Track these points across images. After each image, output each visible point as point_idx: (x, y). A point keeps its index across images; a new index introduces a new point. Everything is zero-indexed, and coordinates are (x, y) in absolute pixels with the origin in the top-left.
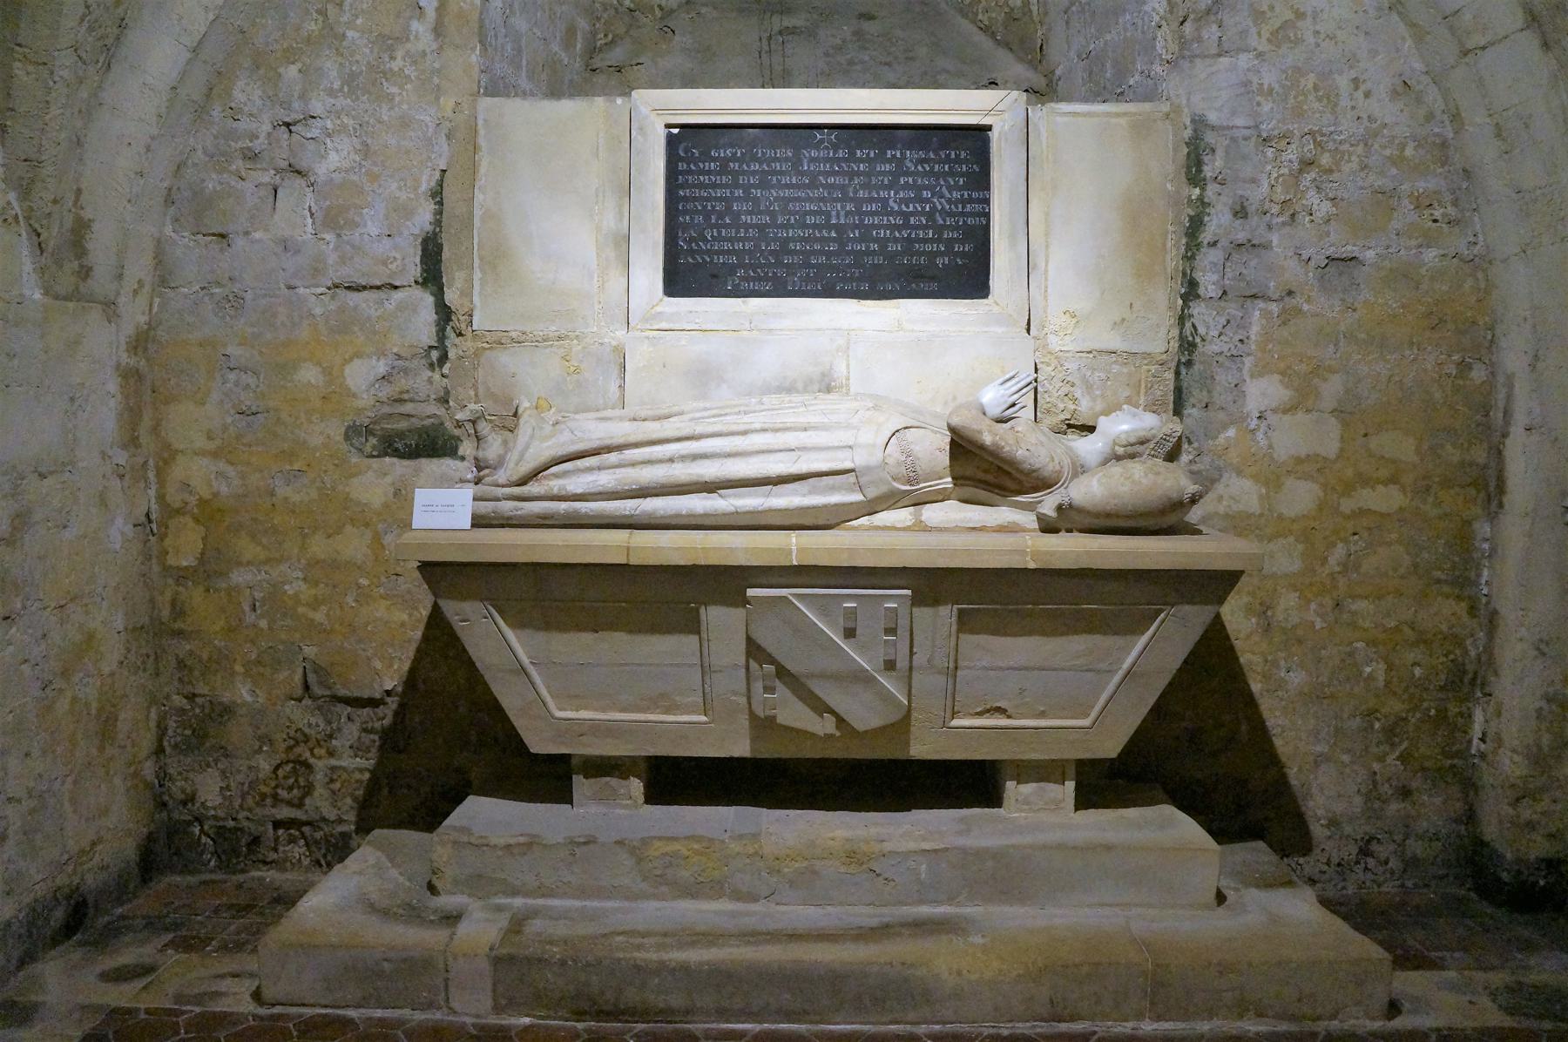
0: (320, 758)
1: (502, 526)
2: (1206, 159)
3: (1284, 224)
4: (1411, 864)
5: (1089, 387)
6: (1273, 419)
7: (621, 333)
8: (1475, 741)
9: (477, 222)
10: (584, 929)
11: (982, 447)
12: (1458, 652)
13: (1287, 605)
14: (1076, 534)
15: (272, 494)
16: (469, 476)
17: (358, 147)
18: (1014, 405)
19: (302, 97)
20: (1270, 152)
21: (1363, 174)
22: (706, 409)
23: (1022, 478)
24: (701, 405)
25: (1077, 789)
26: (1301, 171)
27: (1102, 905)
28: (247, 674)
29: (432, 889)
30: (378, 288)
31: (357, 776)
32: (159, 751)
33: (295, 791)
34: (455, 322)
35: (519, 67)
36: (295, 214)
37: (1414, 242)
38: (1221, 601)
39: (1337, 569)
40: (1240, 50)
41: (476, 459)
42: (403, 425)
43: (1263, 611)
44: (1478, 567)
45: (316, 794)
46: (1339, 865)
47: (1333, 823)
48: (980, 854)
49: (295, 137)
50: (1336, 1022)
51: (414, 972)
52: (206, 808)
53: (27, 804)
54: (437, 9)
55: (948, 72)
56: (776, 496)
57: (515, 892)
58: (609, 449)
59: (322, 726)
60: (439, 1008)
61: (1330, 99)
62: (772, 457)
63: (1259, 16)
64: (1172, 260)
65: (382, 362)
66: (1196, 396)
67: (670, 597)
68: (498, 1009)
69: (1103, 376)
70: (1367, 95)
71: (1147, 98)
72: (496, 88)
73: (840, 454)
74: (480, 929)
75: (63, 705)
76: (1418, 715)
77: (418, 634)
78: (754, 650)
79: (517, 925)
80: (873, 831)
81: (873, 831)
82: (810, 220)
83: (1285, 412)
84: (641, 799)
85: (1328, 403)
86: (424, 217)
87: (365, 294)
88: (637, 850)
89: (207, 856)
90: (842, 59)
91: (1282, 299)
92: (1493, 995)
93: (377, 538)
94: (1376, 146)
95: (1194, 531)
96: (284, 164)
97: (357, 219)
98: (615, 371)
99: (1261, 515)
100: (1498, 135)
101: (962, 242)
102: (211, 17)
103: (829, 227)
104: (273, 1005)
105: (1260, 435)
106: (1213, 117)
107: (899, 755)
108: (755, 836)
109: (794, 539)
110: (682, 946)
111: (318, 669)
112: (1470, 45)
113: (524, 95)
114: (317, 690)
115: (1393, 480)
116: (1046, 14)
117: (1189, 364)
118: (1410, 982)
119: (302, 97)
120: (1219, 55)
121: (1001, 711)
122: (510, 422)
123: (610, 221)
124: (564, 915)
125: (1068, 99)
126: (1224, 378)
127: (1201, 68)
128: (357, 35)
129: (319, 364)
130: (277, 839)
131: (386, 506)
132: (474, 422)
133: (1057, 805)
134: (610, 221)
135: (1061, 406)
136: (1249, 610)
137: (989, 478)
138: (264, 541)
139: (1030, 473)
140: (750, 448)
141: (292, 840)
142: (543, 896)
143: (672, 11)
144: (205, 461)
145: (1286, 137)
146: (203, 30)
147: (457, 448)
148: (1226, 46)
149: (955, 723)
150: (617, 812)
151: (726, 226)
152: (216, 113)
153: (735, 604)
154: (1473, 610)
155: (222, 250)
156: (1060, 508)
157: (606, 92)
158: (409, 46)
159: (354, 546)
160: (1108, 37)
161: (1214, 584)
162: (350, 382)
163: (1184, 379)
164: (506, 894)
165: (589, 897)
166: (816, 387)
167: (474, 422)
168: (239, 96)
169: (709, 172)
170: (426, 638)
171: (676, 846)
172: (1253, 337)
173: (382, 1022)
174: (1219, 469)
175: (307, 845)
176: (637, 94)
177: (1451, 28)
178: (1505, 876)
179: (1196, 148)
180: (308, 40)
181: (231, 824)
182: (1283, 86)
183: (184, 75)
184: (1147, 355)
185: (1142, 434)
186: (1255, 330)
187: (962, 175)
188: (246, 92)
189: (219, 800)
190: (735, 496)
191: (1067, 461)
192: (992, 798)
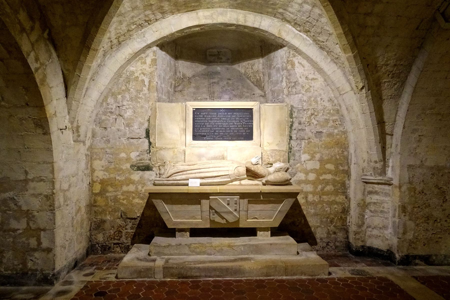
4: (336, 247)
5: (272, 157)
6: (307, 162)
10: (181, 261)
15: (115, 178)
19: (122, 102)
20: (305, 112)
28: (109, 214)
31: (131, 233)
32: (90, 230)
40: (299, 93)
42: (142, 165)
48: (253, 245)
51: (149, 271)
53: (69, 241)
57: (166, 255)
58: (184, 171)
61: (316, 102)
63: (303, 87)
64: (287, 133)
66: (292, 158)
67: (196, 198)
68: (164, 277)
74: (160, 262)
75: (75, 222)
77: (144, 205)
78: (211, 208)
79: (167, 261)
80: (233, 241)
82: (220, 126)
86: (146, 125)
88: (189, 246)
92: (349, 271)
93: (137, 188)
96: (118, 114)
98: (183, 155)
103: (223, 127)
105: (304, 165)
106: (294, 106)
107: (238, 227)
111: (124, 213)
112: (341, 93)
114: (124, 217)
117: (290, 152)
118: (332, 269)
119: (122, 102)
124: (175, 259)
126: (297, 154)
127: (292, 97)
129: (125, 153)
131: (138, 180)
133: (267, 236)
137: (253, 175)
141: (117, 247)
144: (102, 172)
145: (308, 109)
150: (184, 239)
153: (207, 199)
154: (346, 198)
156: (266, 181)
159: (132, 188)
161: (294, 195)
162: (131, 156)
164: (164, 255)
165: (180, 255)
173: (143, 281)
178: (354, 249)
180: (123, 91)
181: (104, 244)
183: (99, 98)
184: (282, 150)
186: (303, 146)
188: (110, 100)
189: (102, 239)
192: (255, 234)
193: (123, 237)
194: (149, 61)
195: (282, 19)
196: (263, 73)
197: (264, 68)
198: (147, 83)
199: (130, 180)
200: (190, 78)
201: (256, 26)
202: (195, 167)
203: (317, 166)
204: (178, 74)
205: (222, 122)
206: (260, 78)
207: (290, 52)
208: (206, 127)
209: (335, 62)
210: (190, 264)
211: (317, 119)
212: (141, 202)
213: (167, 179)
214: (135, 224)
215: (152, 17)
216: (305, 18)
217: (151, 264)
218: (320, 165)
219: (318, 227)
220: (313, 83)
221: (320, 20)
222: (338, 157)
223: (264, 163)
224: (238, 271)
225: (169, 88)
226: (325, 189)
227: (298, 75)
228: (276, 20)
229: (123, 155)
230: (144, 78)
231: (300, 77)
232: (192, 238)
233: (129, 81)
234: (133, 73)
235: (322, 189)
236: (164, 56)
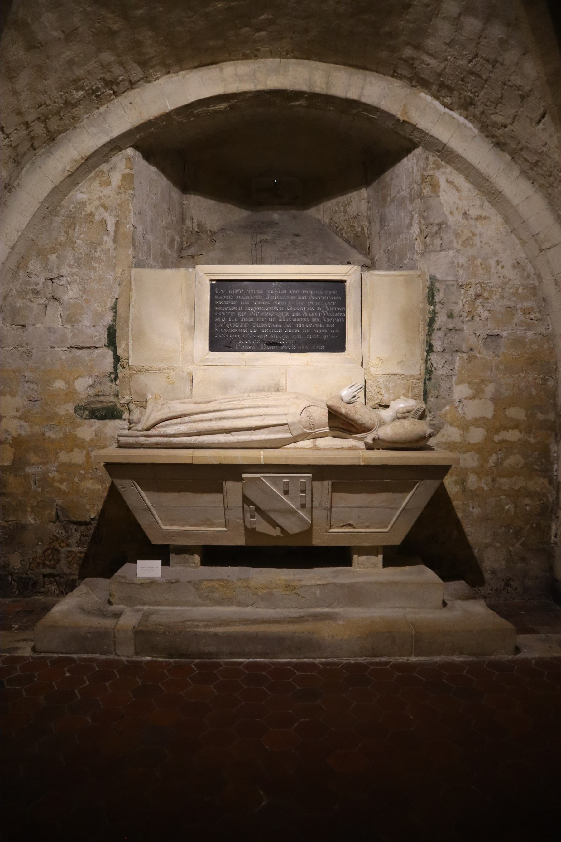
0: (63, 547)
1: (140, 448)
2: (436, 294)
3: (469, 321)
5: (388, 389)
6: (465, 402)
7: (191, 367)
8: (553, 537)
9: (131, 321)
11: (341, 414)
12: (545, 499)
13: (472, 481)
14: (381, 450)
15: (44, 435)
16: (126, 427)
17: (81, 288)
18: (355, 396)
19: (58, 268)
20: (463, 291)
21: (501, 300)
22: (225, 399)
23: (358, 427)
24: (224, 397)
25: (384, 558)
26: (475, 299)
27: (395, 607)
28: (32, 511)
29: (110, 602)
30: (89, 348)
31: (79, 555)
33: (52, 562)
34: (121, 362)
35: (150, 256)
36: (55, 317)
37: (523, 328)
38: (443, 478)
39: (493, 465)
40: (450, 249)
41: (129, 419)
42: (99, 406)
43: (462, 482)
44: (552, 464)
45: (61, 563)
46: (496, 590)
47: (493, 572)
48: (342, 586)
49: (55, 285)
50: (492, 656)
51: (102, 639)
52: (14, 569)
54: (115, 231)
55: (329, 258)
56: (255, 435)
57: (144, 604)
58: (185, 415)
59: (64, 533)
60: (112, 653)
61: (487, 269)
62: (253, 418)
63: (457, 235)
64: (422, 336)
65: (90, 379)
66: (433, 392)
67: (210, 478)
68: (137, 654)
69: (394, 384)
70: (503, 267)
71: (412, 269)
72: (140, 264)
73: (281, 417)
74: (130, 619)
76: (528, 527)
77: (105, 494)
78: (246, 500)
81: (297, 577)
82: (270, 320)
83: (470, 399)
84: (199, 564)
85: (488, 395)
86: (108, 319)
87: (83, 350)
88: (196, 585)
89: (14, 590)
90: (285, 253)
91: (468, 352)
93: (88, 455)
94: (506, 288)
95: (430, 448)
96: (50, 296)
97: (80, 319)
99: (461, 442)
100: (556, 284)
101: (334, 329)
102: (20, 234)
103: (278, 322)
104: (41, 653)
105: (460, 409)
106: (438, 276)
107: (309, 545)
108: (247, 579)
109: (262, 453)
110: (216, 626)
111: (62, 509)
112: (543, 247)
113: (151, 267)
115: (516, 427)
116: (371, 234)
117: (430, 379)
118: (522, 639)
120: (441, 251)
121: (350, 525)
122: (144, 405)
123: (187, 320)
125: (379, 269)
126: (444, 385)
128: (81, 242)
129: (64, 379)
130: (44, 583)
131: (92, 440)
132: (128, 404)
133: (375, 565)
134: (187, 320)
135: (376, 397)
136: (456, 483)
137: (345, 427)
138: (40, 455)
139: (361, 425)
140: (244, 415)
141: (51, 583)
142: (157, 605)
143: (215, 233)
145: (469, 284)
146: (16, 239)
147: (122, 415)
148: (444, 248)
149: (331, 530)
150: (192, 569)
151: (235, 322)
152: (21, 273)
154: (551, 482)
155: (23, 331)
156: (374, 440)
157: (186, 266)
158: (102, 247)
159: (78, 457)
160: (396, 243)
161: (439, 471)
162: (77, 388)
163: (428, 385)
166: (273, 390)
167: (128, 404)
168: (31, 267)
169: (228, 300)
170: (108, 496)
171: (214, 583)
172: (456, 368)
174: (443, 423)
175: (57, 584)
176: (198, 267)
177: (536, 240)
179: (432, 289)
181: (24, 576)
182: (468, 264)
183: (7, 259)
184: (412, 376)
185: (408, 408)
186: (457, 365)
187: (334, 301)
188: (34, 265)
189: (19, 566)
190: (238, 435)
191: (377, 420)
192: (348, 562)
193: (63, 561)
194: (116, 178)
195: (410, 80)
196: (368, 218)
197: (370, 209)
198: (111, 227)
199: (75, 438)
200: (213, 233)
201: (353, 95)
202: (210, 407)
203: (488, 411)
204: (188, 222)
205: (276, 311)
206: (363, 229)
207: (427, 158)
208: (239, 321)
209: (529, 178)
210: (197, 626)
211: (488, 306)
212: (99, 487)
213: (146, 433)
214: (86, 536)
215: (117, 71)
216: (462, 62)
217: (108, 623)
218: (495, 410)
219: (487, 546)
220: (480, 228)
221: (500, 59)
222: (534, 392)
223: (370, 403)
224: (306, 644)
225: (165, 248)
226: (506, 463)
227: (446, 209)
228: (397, 83)
229: (59, 384)
230: (106, 215)
231: (451, 213)
232: (203, 568)
233: (74, 224)
234: (83, 204)
235: (498, 464)
236: (155, 177)
